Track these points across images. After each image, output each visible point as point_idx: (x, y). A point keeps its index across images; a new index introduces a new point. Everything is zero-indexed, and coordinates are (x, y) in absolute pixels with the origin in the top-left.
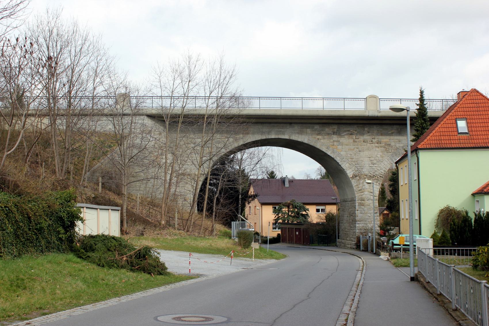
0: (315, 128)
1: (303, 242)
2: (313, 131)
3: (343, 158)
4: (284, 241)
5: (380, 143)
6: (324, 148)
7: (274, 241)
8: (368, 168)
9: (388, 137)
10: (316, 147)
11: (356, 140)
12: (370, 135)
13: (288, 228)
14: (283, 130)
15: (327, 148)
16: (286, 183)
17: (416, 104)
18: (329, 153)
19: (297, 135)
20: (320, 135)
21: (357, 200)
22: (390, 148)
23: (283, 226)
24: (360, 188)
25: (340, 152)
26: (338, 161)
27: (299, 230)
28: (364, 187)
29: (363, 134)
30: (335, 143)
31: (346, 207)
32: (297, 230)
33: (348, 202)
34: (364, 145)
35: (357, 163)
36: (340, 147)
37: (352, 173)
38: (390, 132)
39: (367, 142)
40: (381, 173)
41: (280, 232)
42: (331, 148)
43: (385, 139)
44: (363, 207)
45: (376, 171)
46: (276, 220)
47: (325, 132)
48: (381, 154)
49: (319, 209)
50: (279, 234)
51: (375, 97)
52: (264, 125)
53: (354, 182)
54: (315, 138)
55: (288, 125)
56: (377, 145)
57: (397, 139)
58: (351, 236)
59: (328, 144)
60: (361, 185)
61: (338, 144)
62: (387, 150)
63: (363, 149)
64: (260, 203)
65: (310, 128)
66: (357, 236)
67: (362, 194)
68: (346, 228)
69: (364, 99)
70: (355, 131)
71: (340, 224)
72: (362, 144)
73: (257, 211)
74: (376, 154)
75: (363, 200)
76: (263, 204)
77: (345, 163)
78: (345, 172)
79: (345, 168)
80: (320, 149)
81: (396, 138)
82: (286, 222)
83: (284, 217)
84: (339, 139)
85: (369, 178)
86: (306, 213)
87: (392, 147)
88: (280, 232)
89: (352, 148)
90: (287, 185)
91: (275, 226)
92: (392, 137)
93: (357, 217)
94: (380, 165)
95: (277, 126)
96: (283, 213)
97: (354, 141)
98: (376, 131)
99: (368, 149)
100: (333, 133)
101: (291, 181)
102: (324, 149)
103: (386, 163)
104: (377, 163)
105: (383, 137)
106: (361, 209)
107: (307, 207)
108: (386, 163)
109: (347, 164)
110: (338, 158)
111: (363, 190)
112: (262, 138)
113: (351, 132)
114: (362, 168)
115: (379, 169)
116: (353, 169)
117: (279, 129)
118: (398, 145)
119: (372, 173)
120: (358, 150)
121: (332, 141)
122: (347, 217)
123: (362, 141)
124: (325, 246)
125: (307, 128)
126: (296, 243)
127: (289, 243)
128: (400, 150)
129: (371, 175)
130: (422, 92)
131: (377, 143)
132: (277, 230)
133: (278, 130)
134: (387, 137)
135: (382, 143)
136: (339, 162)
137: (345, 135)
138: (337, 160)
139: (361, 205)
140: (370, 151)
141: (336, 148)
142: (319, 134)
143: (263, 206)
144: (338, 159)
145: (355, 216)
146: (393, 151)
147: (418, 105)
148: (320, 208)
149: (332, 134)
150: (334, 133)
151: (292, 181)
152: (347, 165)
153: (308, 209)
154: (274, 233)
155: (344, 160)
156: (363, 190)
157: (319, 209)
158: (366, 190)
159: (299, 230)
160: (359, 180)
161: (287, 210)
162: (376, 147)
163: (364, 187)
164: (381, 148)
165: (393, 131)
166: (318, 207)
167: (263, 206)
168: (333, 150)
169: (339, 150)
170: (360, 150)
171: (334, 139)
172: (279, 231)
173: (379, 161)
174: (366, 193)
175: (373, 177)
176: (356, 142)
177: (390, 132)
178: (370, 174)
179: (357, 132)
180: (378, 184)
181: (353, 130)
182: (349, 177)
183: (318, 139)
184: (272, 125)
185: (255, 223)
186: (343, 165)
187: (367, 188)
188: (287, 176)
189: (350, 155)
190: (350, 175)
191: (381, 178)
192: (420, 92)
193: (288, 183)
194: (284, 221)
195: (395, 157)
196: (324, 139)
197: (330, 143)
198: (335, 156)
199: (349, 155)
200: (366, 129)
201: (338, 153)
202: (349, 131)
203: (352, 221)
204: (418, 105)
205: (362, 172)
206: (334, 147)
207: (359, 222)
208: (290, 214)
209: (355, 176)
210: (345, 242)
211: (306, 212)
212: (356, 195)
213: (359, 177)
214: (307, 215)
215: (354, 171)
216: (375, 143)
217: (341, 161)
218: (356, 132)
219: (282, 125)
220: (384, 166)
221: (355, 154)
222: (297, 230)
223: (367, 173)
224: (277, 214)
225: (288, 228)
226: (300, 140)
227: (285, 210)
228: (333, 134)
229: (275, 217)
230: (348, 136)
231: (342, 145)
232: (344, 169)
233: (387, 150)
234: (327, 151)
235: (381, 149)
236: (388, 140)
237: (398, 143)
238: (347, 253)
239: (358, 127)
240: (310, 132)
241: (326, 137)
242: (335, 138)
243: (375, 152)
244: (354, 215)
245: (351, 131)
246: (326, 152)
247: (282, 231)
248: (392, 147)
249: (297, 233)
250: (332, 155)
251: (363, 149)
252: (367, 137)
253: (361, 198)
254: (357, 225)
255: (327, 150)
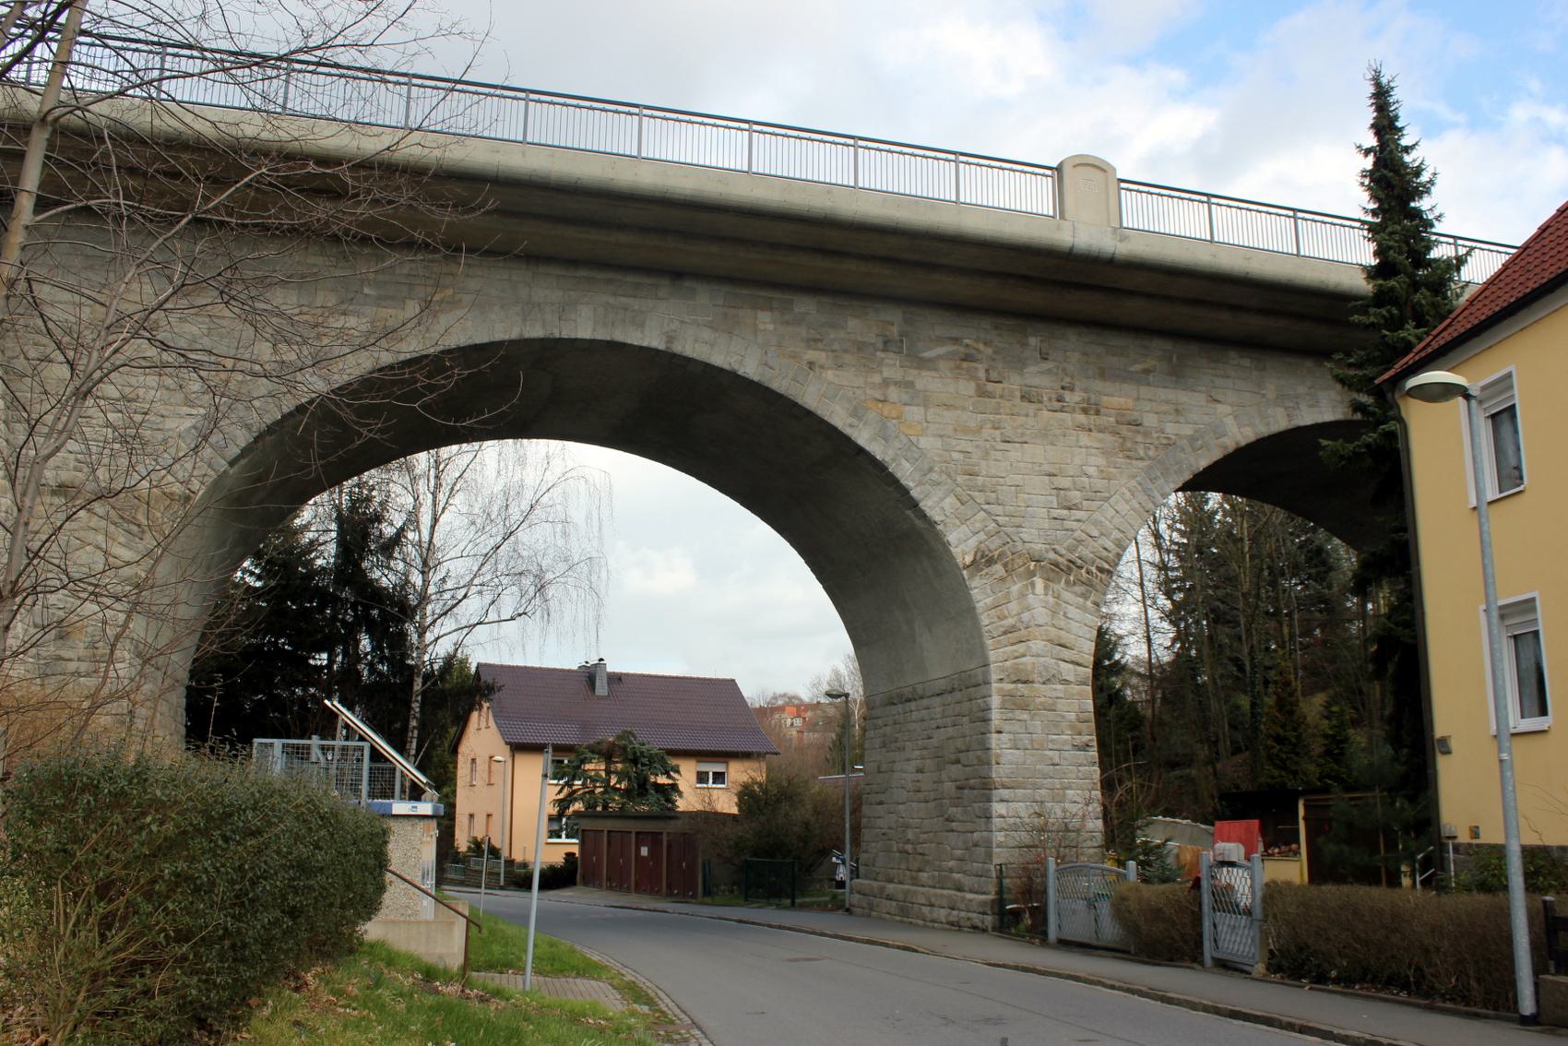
0: (796, 310)
1: (669, 886)
2: (788, 323)
3: (931, 470)
4: (591, 880)
5: (1098, 413)
6: (837, 407)
7: (556, 878)
8: (1046, 526)
9: (1129, 388)
10: (800, 402)
11: (990, 386)
12: (1049, 372)
13: (609, 832)
14: (636, 304)
15: (855, 413)
16: (598, 683)
17: (1360, 147)
18: (863, 437)
19: (707, 334)
20: (820, 345)
21: (994, 677)
22: (1139, 438)
23: (586, 824)
24: (1010, 621)
25: (914, 439)
26: (904, 482)
27: (654, 839)
28: (1026, 616)
29: (1019, 364)
30: (893, 393)
31: (912, 726)
32: (641, 838)
33: (925, 702)
34: (1027, 416)
35: (993, 495)
36: (915, 413)
37: (973, 542)
38: (1138, 367)
39: (1040, 402)
40: (1105, 553)
41: (576, 850)
42: (871, 415)
43: (1118, 398)
44: (1025, 716)
45: (1080, 541)
46: (563, 804)
47: (842, 334)
48: (1101, 461)
49: (707, 773)
50: (570, 856)
51: (1100, 167)
52: (542, 269)
53: (981, 591)
54: (794, 356)
55: (666, 282)
56: (1082, 418)
57: (1167, 402)
58: (952, 863)
59: (859, 392)
60: (1014, 607)
61: (905, 397)
62: (1129, 445)
63: (1023, 434)
64: (507, 743)
65: (771, 309)
66: (996, 861)
67: (1021, 648)
68: (907, 826)
69: (1049, 172)
70: (985, 344)
71: (866, 810)
72: (1016, 410)
73: (496, 779)
74: (1077, 461)
75: (1024, 679)
76: (518, 748)
77: (940, 494)
78: (939, 537)
79: (937, 518)
80: (819, 413)
81: (1163, 397)
82: (599, 809)
83: (593, 791)
84: (912, 374)
85: (1052, 575)
86: (670, 782)
87: (1147, 434)
88: (576, 850)
89: (973, 424)
90: (602, 688)
91: (555, 827)
92: (1145, 391)
93: (995, 767)
94: (1097, 516)
95: (609, 281)
96: (590, 777)
97: (982, 393)
98: (1077, 355)
99: (1045, 435)
100: (885, 343)
101: (616, 679)
102: (838, 417)
103: (1123, 507)
104: (1085, 502)
105: (1108, 384)
106: (1017, 727)
107: (673, 762)
108: (1123, 507)
109: (948, 500)
110: (906, 465)
111: (1023, 632)
112: (527, 335)
113: (967, 345)
114: (1017, 521)
115: (1095, 533)
116: (978, 525)
117: (615, 295)
118: (1171, 429)
119: (1063, 552)
120: (997, 432)
121: (877, 379)
122: (920, 771)
123: (1018, 394)
124: (779, 906)
125: (755, 307)
126: (639, 889)
127: (610, 888)
128: (1183, 450)
129: (1060, 559)
130: (1381, 97)
131: (1085, 411)
132: (564, 840)
133: (611, 300)
134: (1125, 386)
135: (1103, 410)
136: (908, 482)
137: (939, 357)
138: (898, 475)
139: (1015, 703)
140: (1052, 444)
141: (894, 414)
142: (812, 342)
143: (517, 757)
144: (905, 472)
145: (989, 764)
146: (1151, 453)
147: (1367, 152)
148: (712, 768)
149: (880, 345)
150: (887, 344)
151: (620, 679)
152: (950, 502)
153: (678, 766)
154: (557, 851)
155: (934, 476)
156: (1023, 632)
157: (707, 773)
158: (1037, 631)
159: (654, 839)
160: (1002, 579)
161: (603, 767)
162: (1080, 427)
163: (1026, 616)
164: (1101, 435)
165: (1150, 363)
166: (704, 767)
167: (517, 757)
168: (884, 427)
169: (910, 427)
170: (1009, 433)
171: (887, 373)
172: (572, 845)
173: (1094, 495)
174: (1037, 645)
175: (1069, 568)
176: (990, 395)
177: (1138, 367)
178: (1052, 555)
179: (995, 352)
180: (1089, 603)
181: (977, 340)
182: (959, 560)
183: (811, 365)
184: (582, 273)
185: (488, 815)
186: (930, 503)
187: (1040, 621)
188: (601, 660)
189: (960, 456)
190: (964, 553)
191: (1104, 576)
192: (1372, 90)
193: (605, 681)
194: (591, 806)
195: (1162, 480)
196: (840, 366)
197: (869, 392)
198: (891, 452)
199: (955, 455)
200: (1033, 341)
201: (905, 441)
202: (956, 340)
203: (960, 788)
204: (1367, 152)
205: (1019, 544)
206: (886, 409)
207: (1005, 793)
208: (613, 782)
209: (984, 560)
210: (907, 893)
211: (669, 777)
212: (992, 655)
213: (1005, 565)
214: (674, 787)
215: (982, 536)
216: (1073, 411)
217: (920, 483)
218: (989, 351)
219: (631, 278)
220: (1117, 521)
221: (987, 453)
222: (641, 838)
223: (1038, 547)
224: (567, 784)
225: (609, 832)
226: (718, 360)
227: (595, 767)
228: (885, 350)
229: (560, 792)
230: (951, 364)
231: (925, 405)
232: (932, 524)
233: (1129, 445)
234: (851, 426)
235: (1100, 441)
236: (1130, 403)
237: (1171, 418)
238: (1269, 1022)
239: (996, 328)
240: (771, 327)
241: (847, 358)
242: (892, 368)
243: (1077, 450)
244: (971, 757)
245: (966, 341)
246: (848, 431)
247: (583, 845)
248: (1147, 434)
249: (644, 851)
250: (877, 450)
251: (1023, 434)
252: (1037, 376)
253: (1017, 669)
254: (998, 808)
255: (850, 420)
